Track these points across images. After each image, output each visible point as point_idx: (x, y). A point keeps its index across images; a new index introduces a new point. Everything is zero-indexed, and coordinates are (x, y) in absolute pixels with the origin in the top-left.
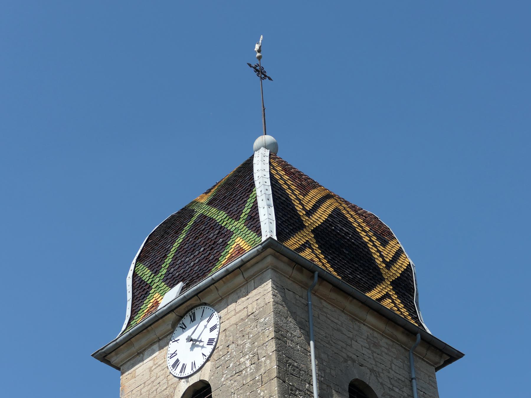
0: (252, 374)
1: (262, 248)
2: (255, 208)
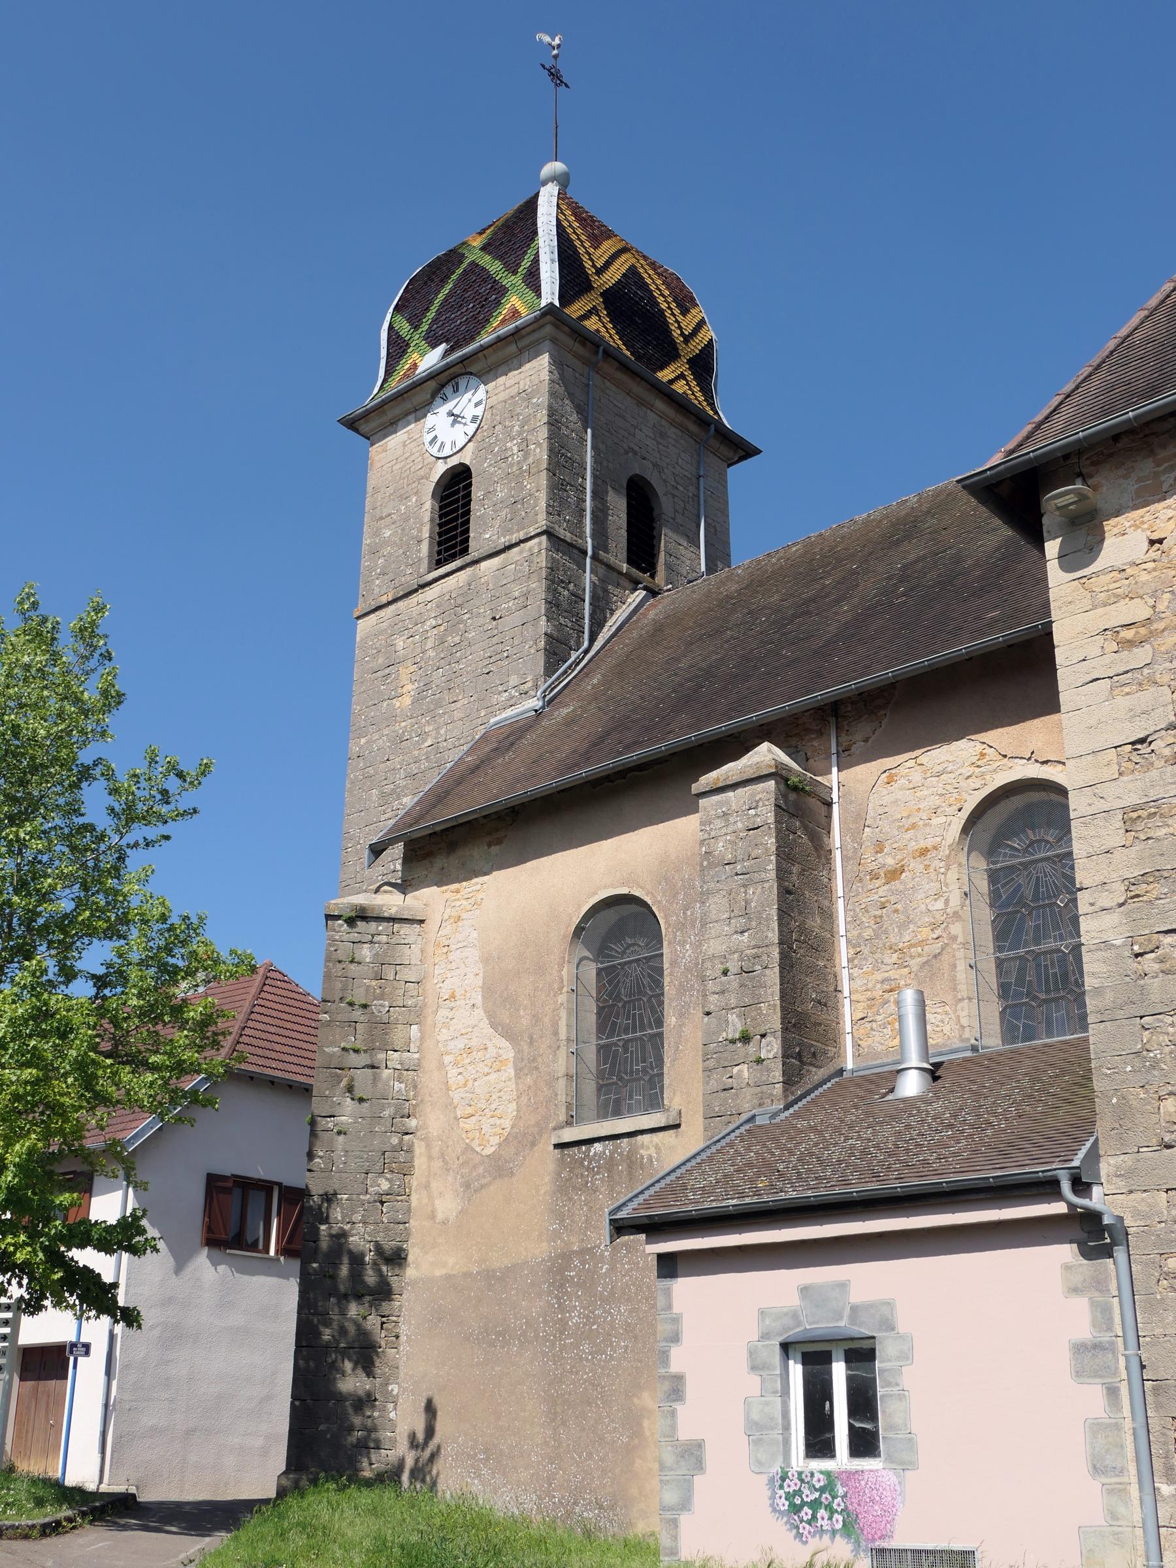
0: (519, 462)
2: (536, 261)
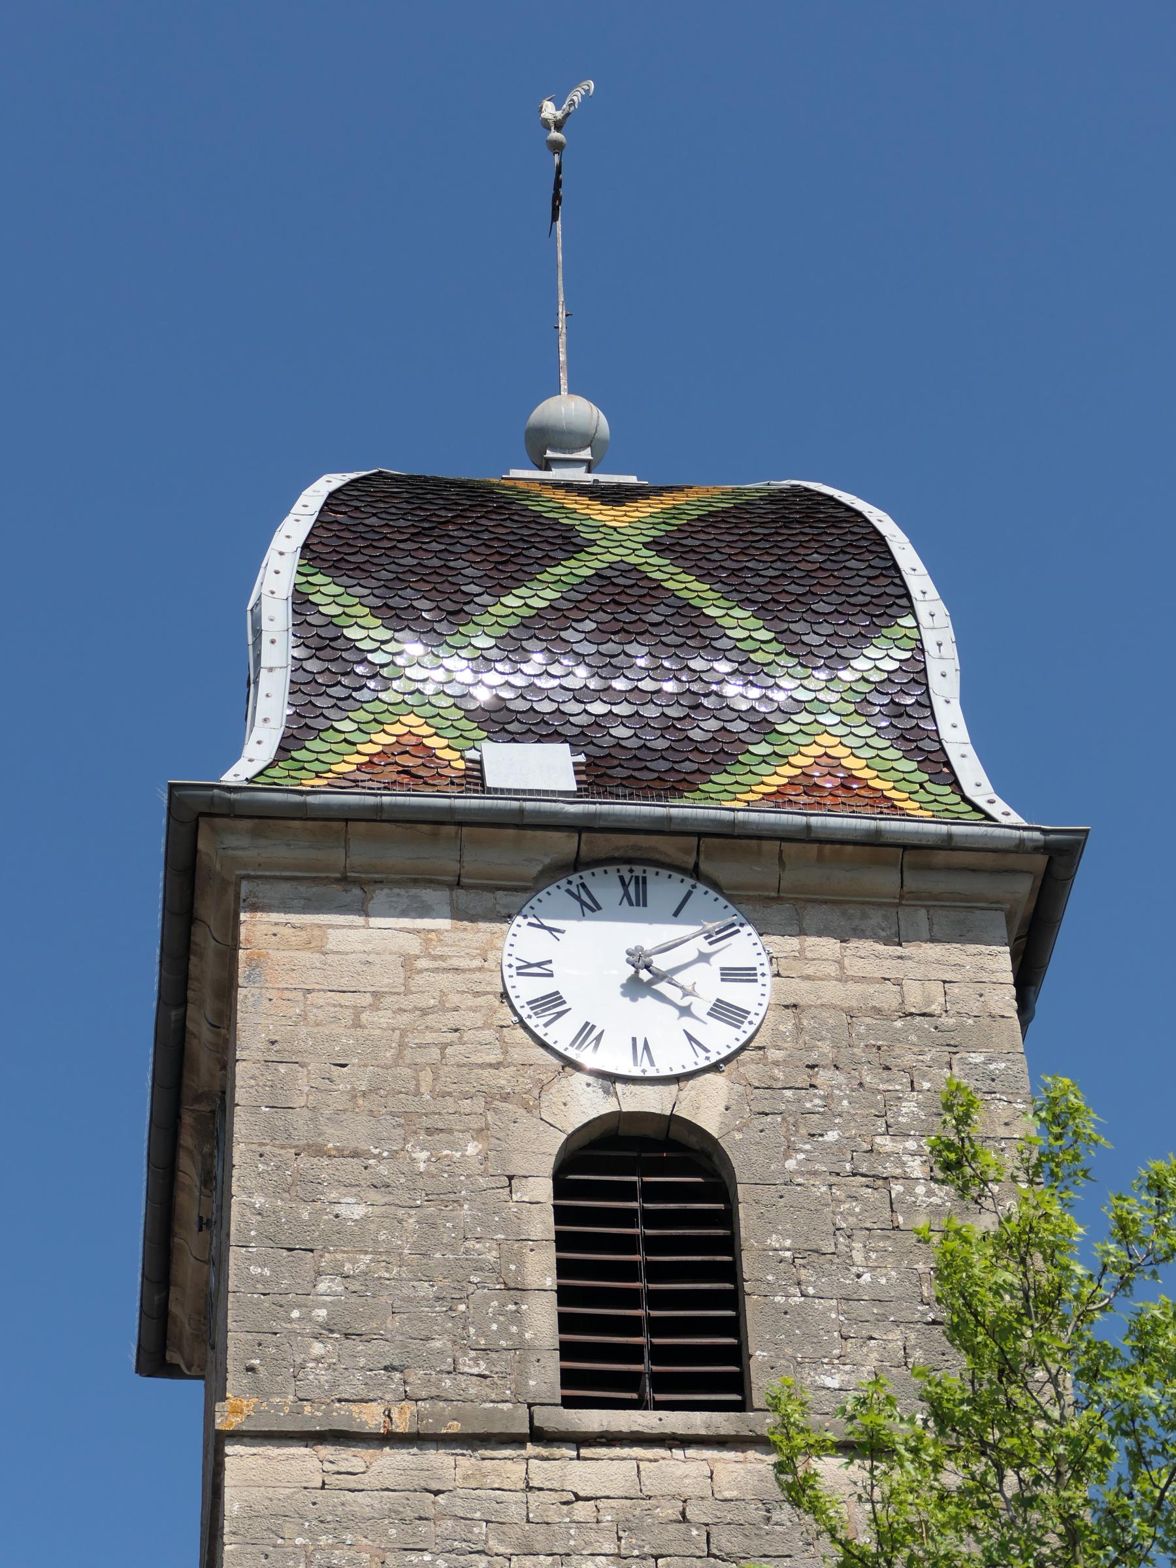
1: (1041, 843)
